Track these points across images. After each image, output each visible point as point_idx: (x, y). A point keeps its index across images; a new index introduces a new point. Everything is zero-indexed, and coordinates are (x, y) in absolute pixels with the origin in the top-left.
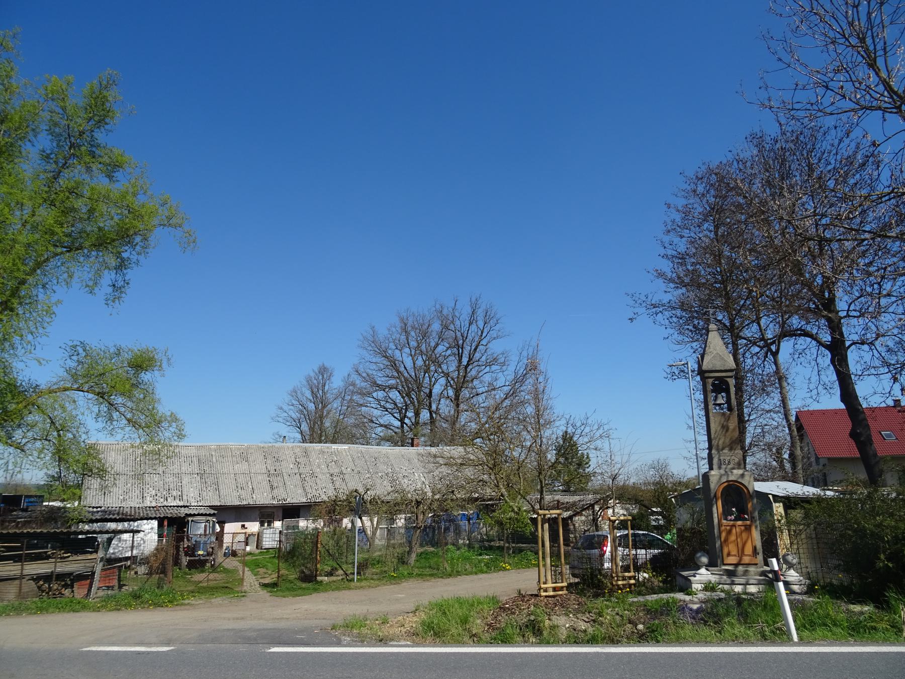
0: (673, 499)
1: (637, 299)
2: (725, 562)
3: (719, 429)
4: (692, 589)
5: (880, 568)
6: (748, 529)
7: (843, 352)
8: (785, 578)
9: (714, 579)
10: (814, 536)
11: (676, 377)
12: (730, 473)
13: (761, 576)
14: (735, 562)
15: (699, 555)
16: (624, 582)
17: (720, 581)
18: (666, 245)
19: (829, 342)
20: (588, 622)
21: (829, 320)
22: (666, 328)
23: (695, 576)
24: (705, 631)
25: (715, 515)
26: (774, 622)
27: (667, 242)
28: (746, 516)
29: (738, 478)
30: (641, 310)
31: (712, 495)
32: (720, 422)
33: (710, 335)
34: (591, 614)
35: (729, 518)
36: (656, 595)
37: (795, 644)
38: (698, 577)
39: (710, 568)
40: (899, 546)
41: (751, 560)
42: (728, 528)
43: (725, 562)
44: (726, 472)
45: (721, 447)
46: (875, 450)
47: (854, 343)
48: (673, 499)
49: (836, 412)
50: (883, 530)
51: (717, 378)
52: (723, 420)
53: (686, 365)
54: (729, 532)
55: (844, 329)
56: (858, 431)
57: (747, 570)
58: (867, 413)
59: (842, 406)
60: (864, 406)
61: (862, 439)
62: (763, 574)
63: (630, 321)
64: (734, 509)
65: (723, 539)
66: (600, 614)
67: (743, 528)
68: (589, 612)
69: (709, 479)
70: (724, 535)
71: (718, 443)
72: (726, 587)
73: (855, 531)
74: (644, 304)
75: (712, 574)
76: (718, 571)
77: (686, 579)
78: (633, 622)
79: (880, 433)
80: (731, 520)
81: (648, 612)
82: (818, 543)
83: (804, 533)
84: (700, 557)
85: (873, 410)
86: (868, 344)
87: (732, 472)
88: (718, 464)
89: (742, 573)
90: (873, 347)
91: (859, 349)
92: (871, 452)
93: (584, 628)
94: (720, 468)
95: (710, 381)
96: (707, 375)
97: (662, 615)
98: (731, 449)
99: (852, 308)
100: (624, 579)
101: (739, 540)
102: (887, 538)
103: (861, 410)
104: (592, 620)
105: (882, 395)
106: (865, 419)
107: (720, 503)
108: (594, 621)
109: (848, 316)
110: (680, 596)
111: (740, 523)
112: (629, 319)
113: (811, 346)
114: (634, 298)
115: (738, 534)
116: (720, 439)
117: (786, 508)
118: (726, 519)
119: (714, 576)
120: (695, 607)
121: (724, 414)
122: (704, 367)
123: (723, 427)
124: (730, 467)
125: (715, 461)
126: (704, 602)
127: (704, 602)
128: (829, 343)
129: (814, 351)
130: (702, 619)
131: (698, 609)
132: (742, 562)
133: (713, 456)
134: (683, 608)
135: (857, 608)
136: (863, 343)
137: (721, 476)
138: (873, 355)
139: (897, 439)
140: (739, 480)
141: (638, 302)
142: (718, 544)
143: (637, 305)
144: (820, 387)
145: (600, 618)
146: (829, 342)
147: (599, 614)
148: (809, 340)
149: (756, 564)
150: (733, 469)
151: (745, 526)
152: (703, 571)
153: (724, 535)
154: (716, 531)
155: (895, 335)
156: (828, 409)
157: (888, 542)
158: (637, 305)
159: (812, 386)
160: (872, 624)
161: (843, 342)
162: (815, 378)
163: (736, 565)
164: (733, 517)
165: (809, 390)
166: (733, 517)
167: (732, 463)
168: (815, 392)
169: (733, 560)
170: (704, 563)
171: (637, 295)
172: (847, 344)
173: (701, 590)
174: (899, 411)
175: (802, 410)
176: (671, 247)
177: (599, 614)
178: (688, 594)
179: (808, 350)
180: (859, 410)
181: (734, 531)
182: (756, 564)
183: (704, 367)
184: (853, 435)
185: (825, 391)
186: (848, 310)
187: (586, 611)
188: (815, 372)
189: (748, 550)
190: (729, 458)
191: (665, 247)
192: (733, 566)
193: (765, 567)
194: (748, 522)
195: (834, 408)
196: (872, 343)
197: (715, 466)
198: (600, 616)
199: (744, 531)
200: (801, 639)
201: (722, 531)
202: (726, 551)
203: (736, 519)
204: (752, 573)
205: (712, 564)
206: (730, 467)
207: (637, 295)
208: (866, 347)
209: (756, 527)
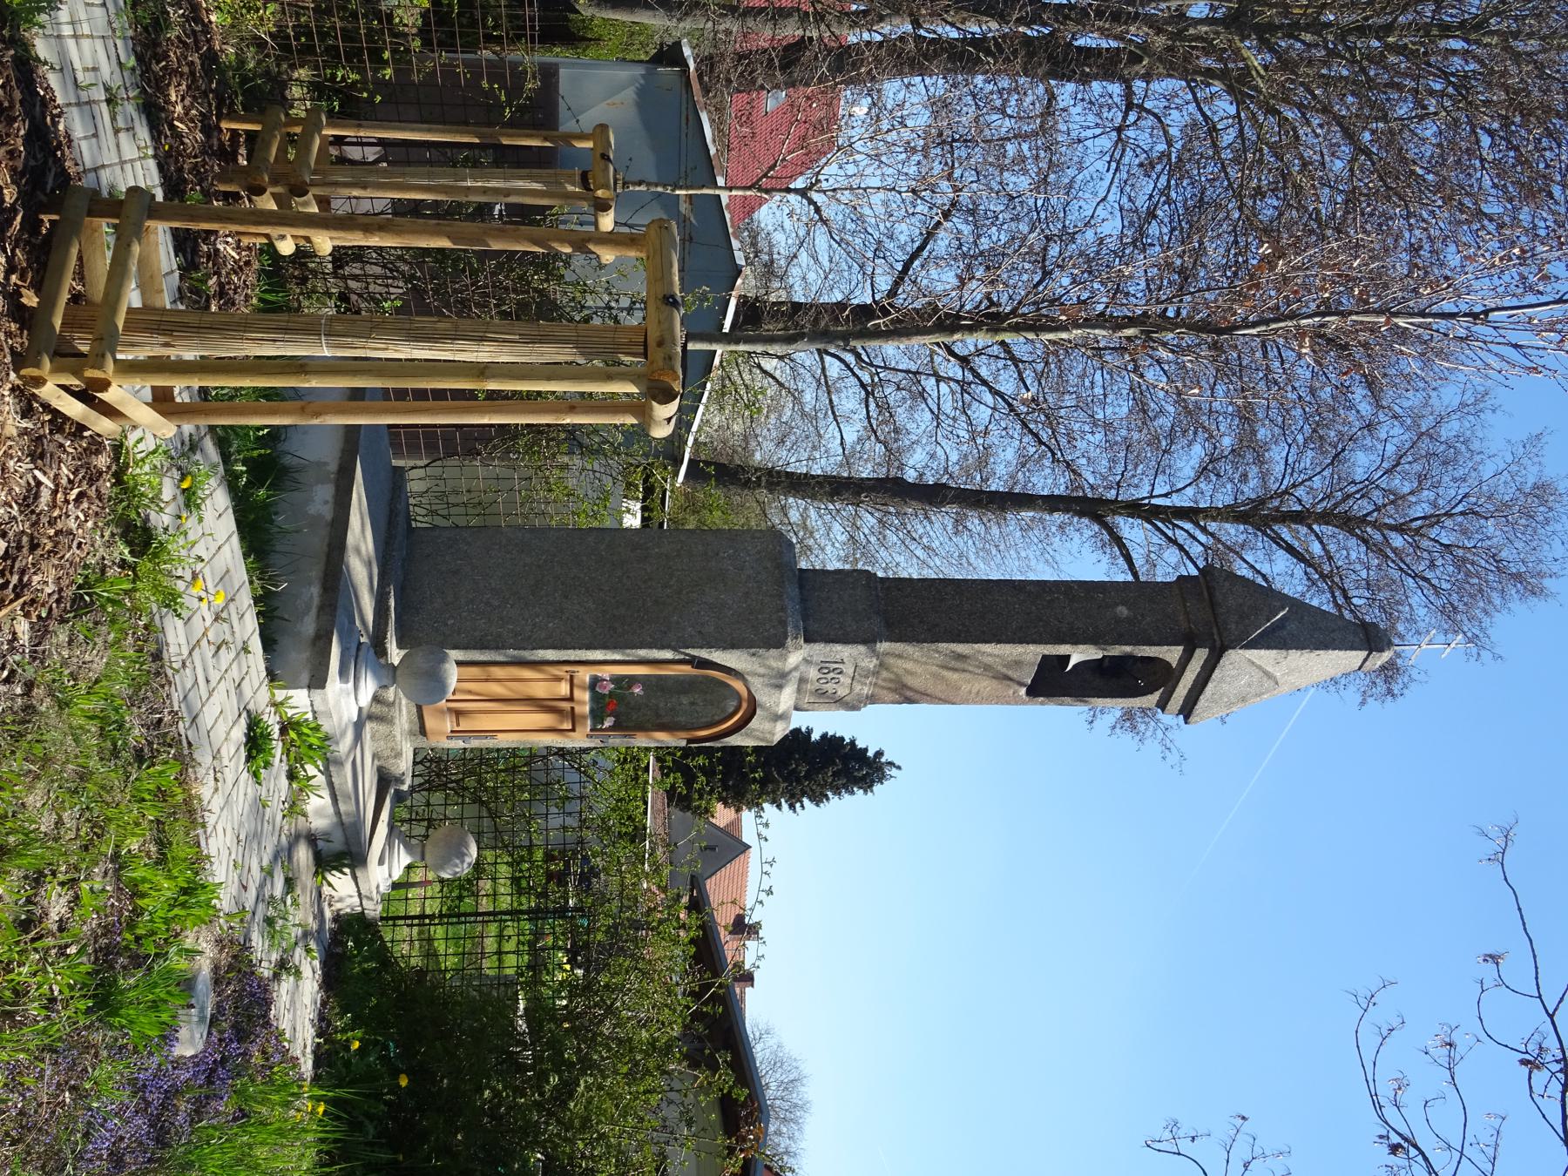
96: (1201, 655)
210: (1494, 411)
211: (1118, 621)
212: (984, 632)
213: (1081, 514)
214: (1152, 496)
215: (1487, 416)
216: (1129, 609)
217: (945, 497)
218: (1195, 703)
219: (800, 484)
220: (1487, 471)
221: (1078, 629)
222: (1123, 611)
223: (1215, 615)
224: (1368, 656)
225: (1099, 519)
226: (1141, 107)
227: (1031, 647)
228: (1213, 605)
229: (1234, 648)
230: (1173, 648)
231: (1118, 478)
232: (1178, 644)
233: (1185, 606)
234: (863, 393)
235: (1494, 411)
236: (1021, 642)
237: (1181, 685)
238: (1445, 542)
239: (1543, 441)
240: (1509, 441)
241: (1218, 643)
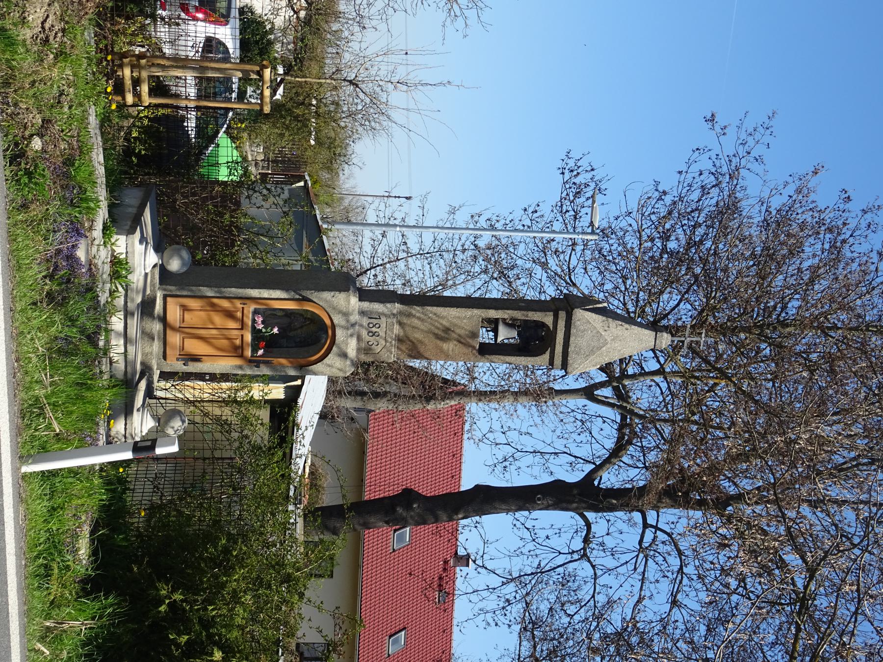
0: (302, 184)
1: (757, 136)
2: (169, 299)
3: (444, 323)
4: (117, 234)
5: (158, 590)
6: (237, 351)
7: (575, 505)
8: (138, 410)
9: (136, 278)
10: (217, 454)
11: (567, 176)
12: (350, 332)
13: (142, 363)
14: (170, 317)
15: (185, 254)
16: (128, 82)
17: (132, 290)
18: (868, 216)
19: (599, 484)
20: (43, 28)
21: (642, 491)
22: (680, 172)
23: (141, 242)
24: (36, 272)
25: (265, 293)
26: (54, 405)
27: (876, 220)
28: (261, 352)
29: (339, 348)
30: (729, 146)
31: (308, 294)
32: (459, 327)
33: (647, 332)
34: (60, 35)
35: (259, 319)
36: (102, 161)
37: (16, 470)
38: (139, 248)
39: (157, 270)
40: (197, 627)
41: (174, 348)
42: (239, 314)
43: (169, 299)
44: (353, 325)
45: (405, 320)
46: (378, 528)
47: (588, 525)
48: (302, 184)
49: (456, 475)
50: (228, 604)
51: (553, 334)
52: (462, 332)
53: (589, 230)
54: (229, 315)
55: (620, 514)
56: (415, 506)
57: (153, 339)
58: (449, 525)
59: (466, 484)
60: (463, 522)
61: (400, 510)
62: (146, 370)
63: (709, 117)
64: (276, 330)
65: (215, 301)
66: (61, 55)
67: (238, 342)
68: (63, 30)
69: (340, 291)
70: (225, 304)
71: (414, 316)
72: (120, 302)
73: (226, 551)
74: (741, 151)
75: (146, 274)
76: (153, 285)
77: (136, 222)
78: (46, 129)
79: (404, 628)
80: (254, 321)
81: (69, 162)
82: (204, 459)
83: (224, 438)
84: (182, 258)
85: (455, 533)
86: (584, 549)
87: (351, 336)
88: (371, 312)
89: (148, 330)
90: (576, 556)
91: (576, 532)
92: (372, 520)
93: (30, 18)
94: (362, 313)
95: (548, 319)
96: (562, 315)
97: (62, 187)
98: (400, 340)
99: (661, 536)
100: (136, 82)
101: (214, 332)
102: (213, 610)
103: (455, 517)
104: (47, 37)
105: (481, 553)
106: (437, 520)
107: (291, 306)
108: (46, 41)
109: (646, 525)
110: (102, 214)
111: (248, 337)
112: (713, 115)
113: (596, 446)
114: (761, 129)
115: (226, 332)
116: (422, 320)
117: (273, 403)
118: (256, 312)
119: (142, 278)
120: (81, 254)
121: (474, 335)
122: (580, 314)
123: (447, 330)
124: (364, 333)
125: (378, 307)
126: (90, 269)
127: (90, 269)
128: (596, 483)
129: (584, 451)
130: (56, 268)
131: (77, 260)
132: (169, 332)
133: (389, 305)
134: (77, 231)
135: (84, 548)
136: (586, 540)
137: (346, 314)
138: (560, 553)
139: (394, 551)
140: (334, 348)
141: (750, 139)
142: (209, 292)
143: (743, 136)
144: (509, 450)
145: (52, 56)
146: (599, 484)
147: (62, 53)
148: (610, 444)
149: (165, 357)
150: (359, 339)
151: (242, 347)
152: (153, 258)
153: (225, 304)
154: (234, 291)
155: (593, 596)
156: (463, 466)
157: (206, 609)
158: (743, 136)
159: (513, 436)
160: (56, 571)
161: (597, 510)
162: (529, 443)
163: (163, 319)
164: (260, 327)
165: (506, 429)
166: (260, 327)
167: (372, 340)
168: (501, 439)
169: (174, 314)
170: (168, 262)
171: (767, 139)
172: (590, 515)
173: (113, 251)
174: (446, 562)
175: (465, 436)
176: (864, 224)
177: (62, 53)
178: (105, 228)
179: (589, 438)
180: (457, 514)
181: (232, 324)
182: (165, 357)
183: (580, 314)
184: (408, 496)
185: (500, 458)
186: (656, 528)
187: (67, 23)
188: (540, 447)
189: (195, 347)
190: (382, 334)
191: (865, 212)
192: (162, 311)
193: (158, 372)
194: (248, 353)
195: (464, 452)
196: (584, 556)
197: (366, 305)
198: (56, 58)
199: (233, 343)
200: (24, 476)
201: (232, 302)
202: (193, 303)
203: (255, 332)
204: (148, 350)
205: (165, 276)
206: (364, 333)
207: (767, 139)
208: (577, 544)
209: (240, 367)
230: (548, 313)
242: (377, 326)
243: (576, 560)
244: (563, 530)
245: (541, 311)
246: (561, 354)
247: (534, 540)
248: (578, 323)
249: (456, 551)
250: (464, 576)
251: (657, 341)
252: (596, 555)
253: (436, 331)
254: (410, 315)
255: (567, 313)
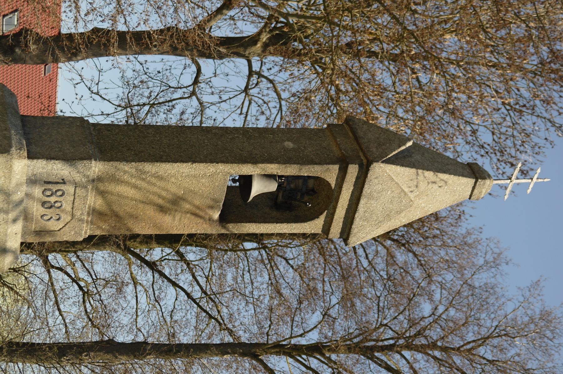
3: (174, 189)
96: (353, 170)
109: (251, 73)
138: (170, 87)
210: (507, 264)
211: (286, 150)
212: (181, 156)
213: (243, 355)
214: (291, 337)
215: (503, 267)
216: (294, 143)
217: (145, 350)
218: (352, 223)
219: (35, 350)
220: (510, 307)
221: (256, 154)
222: (289, 145)
223: (359, 145)
224: (476, 183)
225: (255, 357)
226: (260, 75)
227: (221, 167)
228: (356, 139)
229: (377, 161)
230: (331, 166)
231: (268, 329)
232: (333, 163)
233: (336, 141)
234: (81, 293)
235: (507, 264)
236: (212, 162)
237: (339, 205)
238: (490, 358)
239: (541, 285)
240: (519, 288)
241: (365, 161)
242: (59, 193)
243: (186, 98)
244: (173, 67)
245: (320, 163)
246: (342, 220)
247: (146, 74)
248: (376, 181)
249: (60, 30)
250: (79, 99)
251: (476, 191)
252: (204, 90)
253: (160, 201)
254: (113, 179)
255: (361, 166)
